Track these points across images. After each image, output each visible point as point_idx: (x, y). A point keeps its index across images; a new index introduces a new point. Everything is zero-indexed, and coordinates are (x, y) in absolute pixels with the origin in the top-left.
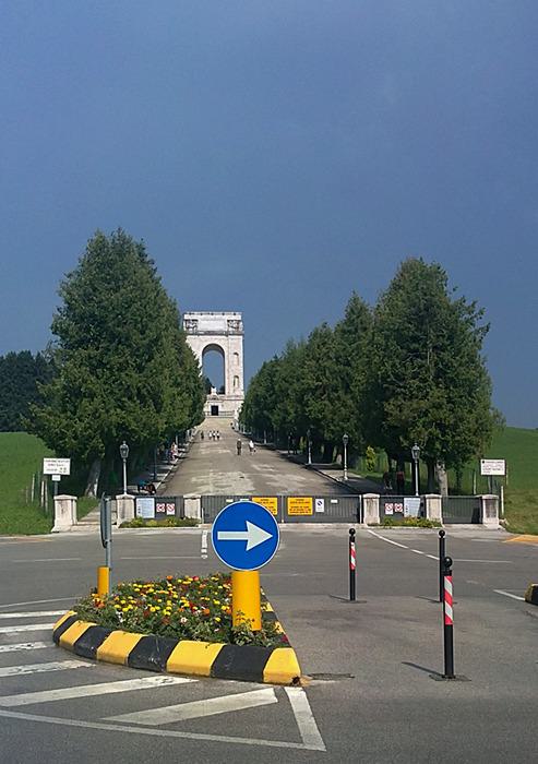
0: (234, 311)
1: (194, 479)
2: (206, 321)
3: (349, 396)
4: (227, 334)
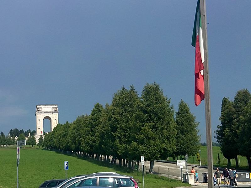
0: (55, 104)
1: (133, 160)
2: (45, 108)
3: (184, 136)
4: (52, 113)
